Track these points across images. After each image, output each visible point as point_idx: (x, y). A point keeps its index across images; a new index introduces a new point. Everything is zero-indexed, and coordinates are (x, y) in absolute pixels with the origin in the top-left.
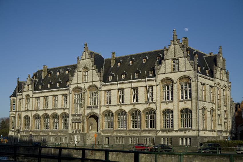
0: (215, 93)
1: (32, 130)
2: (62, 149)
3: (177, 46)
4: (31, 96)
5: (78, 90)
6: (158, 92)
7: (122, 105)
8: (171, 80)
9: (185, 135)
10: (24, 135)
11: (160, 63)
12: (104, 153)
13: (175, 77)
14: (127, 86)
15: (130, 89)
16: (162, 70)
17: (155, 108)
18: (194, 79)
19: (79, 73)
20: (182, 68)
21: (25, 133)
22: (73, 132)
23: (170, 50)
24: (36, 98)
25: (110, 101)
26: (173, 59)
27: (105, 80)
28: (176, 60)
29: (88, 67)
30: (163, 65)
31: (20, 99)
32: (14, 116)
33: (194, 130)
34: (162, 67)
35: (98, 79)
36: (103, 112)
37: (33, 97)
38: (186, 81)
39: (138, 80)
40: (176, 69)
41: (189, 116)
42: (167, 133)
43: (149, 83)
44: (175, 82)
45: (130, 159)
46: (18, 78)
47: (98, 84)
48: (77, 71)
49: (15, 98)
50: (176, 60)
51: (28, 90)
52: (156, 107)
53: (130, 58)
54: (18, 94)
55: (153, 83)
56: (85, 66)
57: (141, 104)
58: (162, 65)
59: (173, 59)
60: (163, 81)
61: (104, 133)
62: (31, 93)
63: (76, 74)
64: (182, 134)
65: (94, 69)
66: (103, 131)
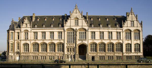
0: (137, 37)
1: (31, 52)
2: (71, 66)
3: (133, 15)
4: (29, 30)
5: (71, 30)
6: (123, 35)
7: (44, 40)
8: (130, 31)
9: (137, 55)
10: (24, 55)
11: (124, 22)
12: (97, 66)
13: (132, 29)
14: (106, 31)
15: (41, 32)
16: (126, 25)
17: (122, 43)
18: (141, 31)
19: (71, 20)
20: (135, 25)
21: (25, 54)
22: (68, 53)
23: (130, 17)
24: (35, 32)
25: (45, 37)
26: (131, 21)
27: (90, 26)
28: (132, 22)
29: (78, 18)
30: (126, 23)
31: (18, 33)
32: (13, 43)
33: (142, 53)
34: (125, 24)
35: (86, 25)
36: (90, 43)
37: (32, 31)
38: (26, 32)
39: (37, 28)
40: (133, 25)
41: (129, 47)
42: (129, 54)
43: (119, 31)
44: (132, 31)
45: (96, 67)
46: (87, 13)
47: (86, 28)
48: (70, 19)
49: (13, 31)
50: (26, 24)
51: (27, 26)
52: (123, 42)
53: (101, 17)
54: (16, 29)
55: (121, 31)
56: (76, 17)
57: (114, 40)
58: (126, 23)
59: (131, 21)
60: (126, 30)
61: (91, 54)
62: (29, 29)
63: (69, 21)
64: (136, 54)
65: (83, 19)
66: (89, 53)
